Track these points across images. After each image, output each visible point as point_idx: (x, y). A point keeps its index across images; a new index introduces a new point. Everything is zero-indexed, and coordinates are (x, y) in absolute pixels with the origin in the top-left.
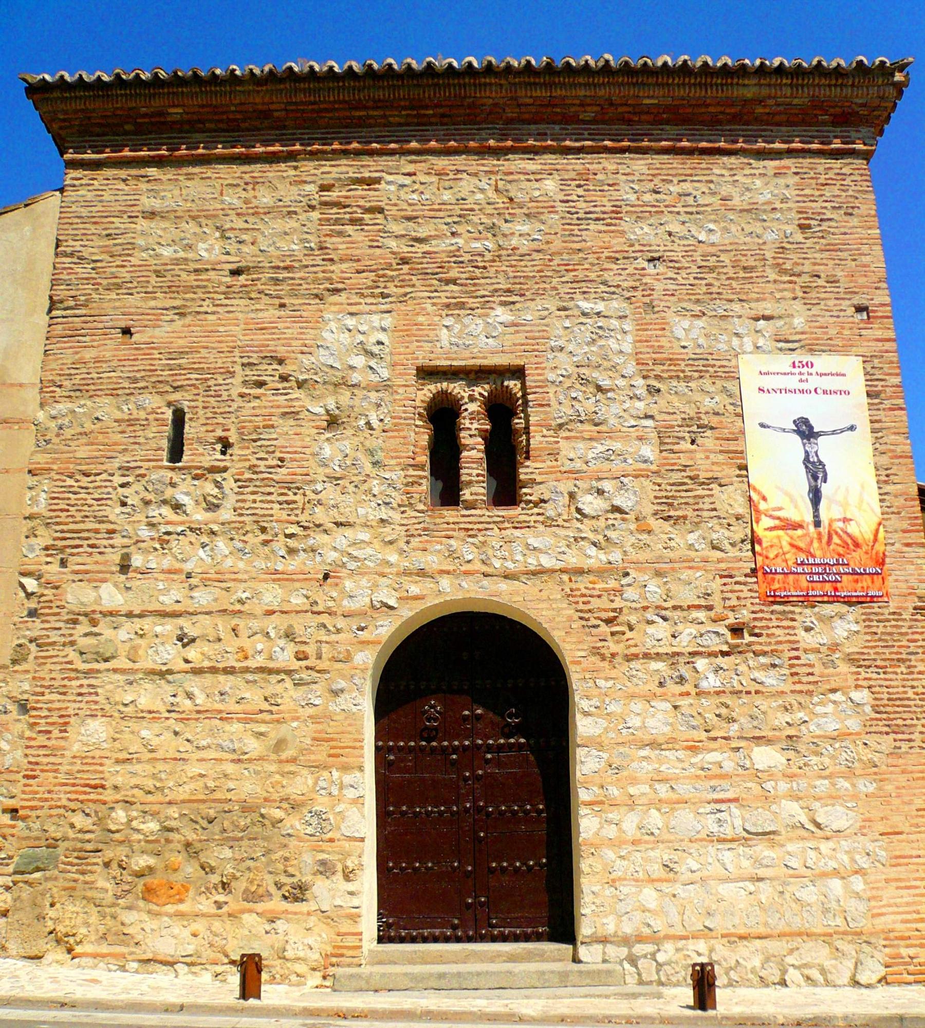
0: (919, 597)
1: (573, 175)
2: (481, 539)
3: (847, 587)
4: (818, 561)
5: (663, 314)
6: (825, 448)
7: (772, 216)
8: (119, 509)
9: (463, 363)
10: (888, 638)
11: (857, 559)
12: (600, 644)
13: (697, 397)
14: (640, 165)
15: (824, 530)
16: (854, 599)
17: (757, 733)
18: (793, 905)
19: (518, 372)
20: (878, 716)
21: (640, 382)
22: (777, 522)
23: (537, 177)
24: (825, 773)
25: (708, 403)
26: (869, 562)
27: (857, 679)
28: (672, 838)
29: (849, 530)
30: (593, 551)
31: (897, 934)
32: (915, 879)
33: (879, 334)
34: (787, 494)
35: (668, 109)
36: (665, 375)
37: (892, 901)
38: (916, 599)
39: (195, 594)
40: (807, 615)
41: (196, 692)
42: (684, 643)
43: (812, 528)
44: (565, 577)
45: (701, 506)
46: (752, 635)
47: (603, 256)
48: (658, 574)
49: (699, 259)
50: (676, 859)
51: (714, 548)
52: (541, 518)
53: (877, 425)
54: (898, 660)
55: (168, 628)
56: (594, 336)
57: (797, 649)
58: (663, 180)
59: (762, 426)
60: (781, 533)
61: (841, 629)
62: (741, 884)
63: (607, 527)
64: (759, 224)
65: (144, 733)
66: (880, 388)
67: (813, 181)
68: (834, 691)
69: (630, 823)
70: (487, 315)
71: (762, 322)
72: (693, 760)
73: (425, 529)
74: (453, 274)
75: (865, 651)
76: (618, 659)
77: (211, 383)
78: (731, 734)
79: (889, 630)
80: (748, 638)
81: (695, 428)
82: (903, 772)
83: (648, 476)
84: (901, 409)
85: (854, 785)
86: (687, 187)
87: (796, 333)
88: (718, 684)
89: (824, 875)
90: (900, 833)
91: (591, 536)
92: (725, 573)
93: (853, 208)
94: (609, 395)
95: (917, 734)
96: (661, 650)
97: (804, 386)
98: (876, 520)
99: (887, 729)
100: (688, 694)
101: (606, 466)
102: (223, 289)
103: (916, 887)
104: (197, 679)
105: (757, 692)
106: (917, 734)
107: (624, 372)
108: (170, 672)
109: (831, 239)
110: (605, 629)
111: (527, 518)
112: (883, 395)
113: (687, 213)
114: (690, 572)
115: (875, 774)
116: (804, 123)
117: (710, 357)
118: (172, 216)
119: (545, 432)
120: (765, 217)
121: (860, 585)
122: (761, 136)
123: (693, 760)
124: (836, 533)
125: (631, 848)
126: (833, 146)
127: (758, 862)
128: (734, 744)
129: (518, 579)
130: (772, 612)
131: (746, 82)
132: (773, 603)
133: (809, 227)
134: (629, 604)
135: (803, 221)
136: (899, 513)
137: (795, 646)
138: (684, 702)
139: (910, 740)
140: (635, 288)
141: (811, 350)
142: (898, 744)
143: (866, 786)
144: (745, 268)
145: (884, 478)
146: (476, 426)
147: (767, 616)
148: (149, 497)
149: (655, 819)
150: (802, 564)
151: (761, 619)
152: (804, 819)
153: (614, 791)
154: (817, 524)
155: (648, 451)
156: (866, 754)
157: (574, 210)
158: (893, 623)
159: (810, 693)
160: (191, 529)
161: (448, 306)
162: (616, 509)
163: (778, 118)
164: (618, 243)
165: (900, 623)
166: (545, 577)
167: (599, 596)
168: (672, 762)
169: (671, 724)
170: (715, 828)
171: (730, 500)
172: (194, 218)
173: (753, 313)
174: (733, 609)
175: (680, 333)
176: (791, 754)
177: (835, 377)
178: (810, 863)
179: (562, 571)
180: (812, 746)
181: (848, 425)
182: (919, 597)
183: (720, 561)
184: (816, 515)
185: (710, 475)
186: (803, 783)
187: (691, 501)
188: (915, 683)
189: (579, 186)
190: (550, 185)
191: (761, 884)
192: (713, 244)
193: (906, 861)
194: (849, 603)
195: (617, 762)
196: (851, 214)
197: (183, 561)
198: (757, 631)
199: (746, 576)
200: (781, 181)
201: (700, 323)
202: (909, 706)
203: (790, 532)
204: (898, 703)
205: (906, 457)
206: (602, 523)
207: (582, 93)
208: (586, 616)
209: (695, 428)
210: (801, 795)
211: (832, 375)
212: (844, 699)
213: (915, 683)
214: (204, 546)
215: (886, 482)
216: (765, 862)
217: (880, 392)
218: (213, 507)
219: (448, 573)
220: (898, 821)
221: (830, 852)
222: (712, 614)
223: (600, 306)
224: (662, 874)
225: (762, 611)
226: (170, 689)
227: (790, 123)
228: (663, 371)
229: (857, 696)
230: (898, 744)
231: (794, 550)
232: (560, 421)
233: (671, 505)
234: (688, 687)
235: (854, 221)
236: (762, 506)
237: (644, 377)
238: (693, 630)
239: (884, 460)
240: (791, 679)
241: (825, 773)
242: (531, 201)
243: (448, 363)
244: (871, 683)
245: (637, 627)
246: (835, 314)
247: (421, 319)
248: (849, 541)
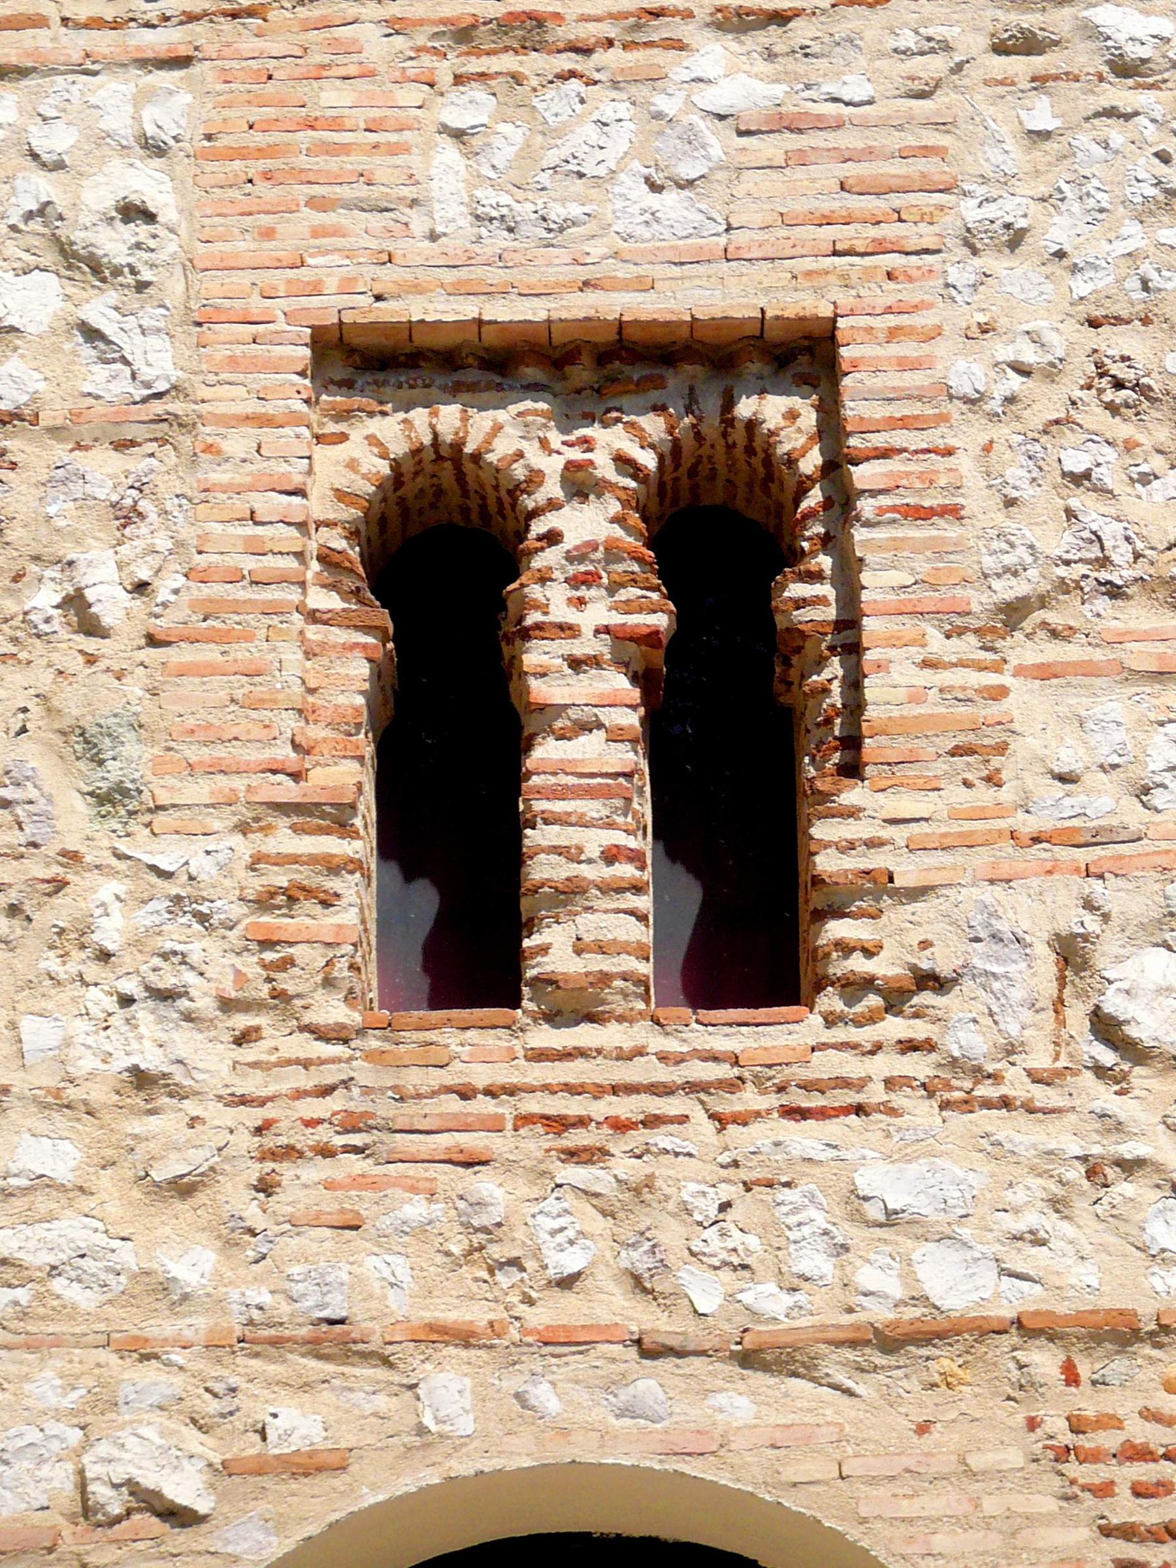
2: (624, 1166)
9: (533, 311)
19: (806, 355)
44: (1045, 1361)
52: (919, 1066)
119: (937, 644)
166: (945, 1360)
179: (1026, 1328)
219: (465, 1338)
232: (1008, 590)
243: (467, 309)
247: (332, 97)
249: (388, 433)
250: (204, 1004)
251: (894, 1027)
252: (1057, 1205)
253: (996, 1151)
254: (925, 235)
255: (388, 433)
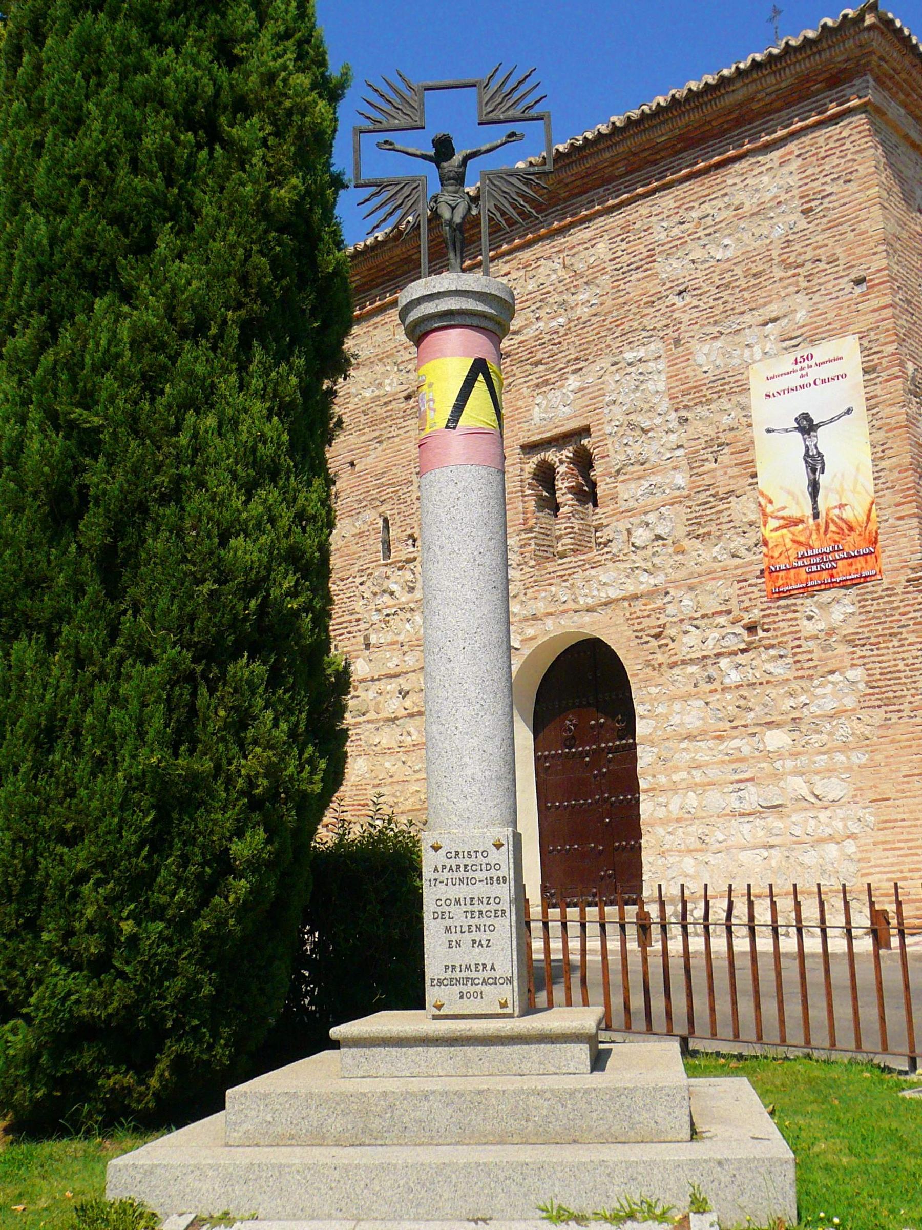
0: (913, 569)
1: (618, 231)
2: (571, 582)
3: (843, 571)
4: (816, 552)
5: (688, 345)
6: (824, 440)
7: (779, 211)
8: (362, 602)
9: (548, 434)
10: (881, 614)
11: (852, 543)
12: (651, 657)
13: (716, 417)
14: (667, 201)
15: (821, 521)
16: (849, 583)
17: (769, 719)
18: (798, 868)
19: (585, 431)
20: (871, 691)
21: (673, 415)
22: (782, 522)
23: (591, 243)
24: (824, 749)
25: (726, 421)
26: (862, 543)
27: (853, 659)
28: (704, 815)
29: (844, 516)
30: (644, 577)
31: (882, 892)
32: (899, 841)
33: (875, 304)
34: (789, 493)
35: (680, 138)
36: (691, 404)
37: (879, 862)
38: (909, 572)
39: (406, 658)
40: (808, 605)
41: (412, 730)
42: (710, 648)
43: (811, 521)
44: (626, 604)
45: (721, 520)
46: (764, 631)
47: (642, 303)
48: (691, 588)
49: (716, 279)
50: (707, 832)
51: (733, 556)
52: (609, 556)
53: (873, 402)
54: (891, 635)
55: (391, 686)
56: (637, 383)
57: (799, 638)
58: (686, 209)
59: (768, 431)
60: (785, 531)
61: (837, 614)
62: (757, 851)
63: (653, 554)
64: (767, 223)
65: (387, 765)
66: (876, 361)
67: (814, 158)
68: (832, 672)
69: (675, 803)
70: (562, 386)
71: (770, 325)
72: (721, 748)
73: (535, 581)
74: (539, 356)
75: (860, 630)
76: (664, 668)
77: (400, 493)
78: (749, 722)
79: (882, 607)
80: (761, 633)
81: (715, 448)
82: (892, 742)
83: (681, 502)
84: (897, 377)
85: (848, 758)
86: (707, 208)
87: (799, 328)
88: (738, 679)
89: (821, 841)
90: (888, 799)
91: (644, 565)
92: (741, 578)
93: (851, 173)
94: (650, 434)
95: (906, 704)
96: (694, 656)
97: (805, 381)
98: (869, 500)
99: (879, 703)
100: (716, 691)
101: (651, 499)
102: (401, 414)
103: (900, 849)
104: (411, 721)
105: (768, 682)
106: (906, 704)
107: (660, 411)
108: (396, 718)
109: (832, 215)
110: (654, 643)
111: (599, 558)
112: (879, 368)
113: (706, 235)
114: (714, 582)
115: (867, 746)
116: (802, 99)
117: (726, 375)
118: (368, 362)
119: (608, 480)
120: (772, 215)
121: (854, 567)
122: (763, 130)
123: (721, 748)
124: (833, 521)
125: (676, 825)
126: (829, 113)
127: (770, 833)
128: (751, 730)
129: (595, 611)
130: (778, 608)
131: (732, 88)
132: (779, 598)
133: (811, 210)
134: (670, 619)
135: (805, 206)
136: (893, 487)
137: (797, 636)
138: (712, 698)
139: (899, 711)
140: (667, 326)
141: (812, 341)
142: (889, 715)
143: (859, 758)
144: (754, 275)
145: (880, 452)
146: (566, 485)
147: (773, 611)
148: (376, 589)
149: (692, 799)
150: (803, 557)
151: (769, 615)
152: (805, 792)
153: (662, 779)
154: (816, 516)
155: (681, 479)
156: (860, 729)
157: (618, 266)
158: (887, 599)
159: (811, 677)
160: (401, 610)
161: (537, 386)
162: (658, 537)
163: (777, 104)
164: (652, 287)
165: (892, 598)
166: (613, 606)
167: (649, 616)
168: (703, 751)
169: (703, 719)
170: (736, 805)
171: (743, 509)
172: (380, 360)
173: (761, 320)
174: (746, 610)
175: (701, 359)
176: (796, 735)
177: (833, 363)
178: (809, 831)
179: (624, 599)
180: (813, 726)
181: (845, 409)
182: (913, 569)
183: (736, 568)
184: (815, 507)
185: (727, 489)
186: (804, 759)
187: (714, 517)
188: (905, 655)
189: (622, 240)
190: (602, 247)
191: (772, 851)
192: (728, 260)
193: (891, 824)
194: (846, 587)
195: (664, 755)
196: (850, 181)
197: (398, 634)
198: (766, 627)
199: (757, 577)
200: (785, 170)
201: (718, 344)
202: (900, 678)
203: (792, 529)
204: (889, 676)
205: (901, 427)
206: (649, 552)
207: (607, 155)
208: (639, 634)
209: (715, 448)
210: (804, 770)
211: (830, 361)
212: (841, 678)
213: (905, 655)
214: (408, 620)
215: (882, 458)
216: (774, 831)
217: (876, 365)
218: (412, 590)
219: (551, 614)
220: (887, 789)
221: (828, 820)
222: (731, 617)
223: (642, 353)
224: (698, 845)
225: (770, 608)
226: (398, 731)
227: (789, 105)
228: (689, 400)
229: (852, 674)
230: (889, 715)
231: (796, 546)
232: (617, 468)
233: (699, 524)
234: (716, 685)
235: (853, 187)
236: (769, 509)
237: (676, 410)
238: (715, 634)
239: (880, 436)
240: (794, 667)
241: (824, 749)
242: (589, 268)
243: (540, 437)
244: (866, 660)
245: (678, 638)
246: (834, 295)
247: (520, 403)
248: (844, 526)
249: (535, 459)
250: (515, 566)
251: (606, 550)
252: (627, 576)
253: (618, 569)
254: (601, 405)
255: (535, 459)
